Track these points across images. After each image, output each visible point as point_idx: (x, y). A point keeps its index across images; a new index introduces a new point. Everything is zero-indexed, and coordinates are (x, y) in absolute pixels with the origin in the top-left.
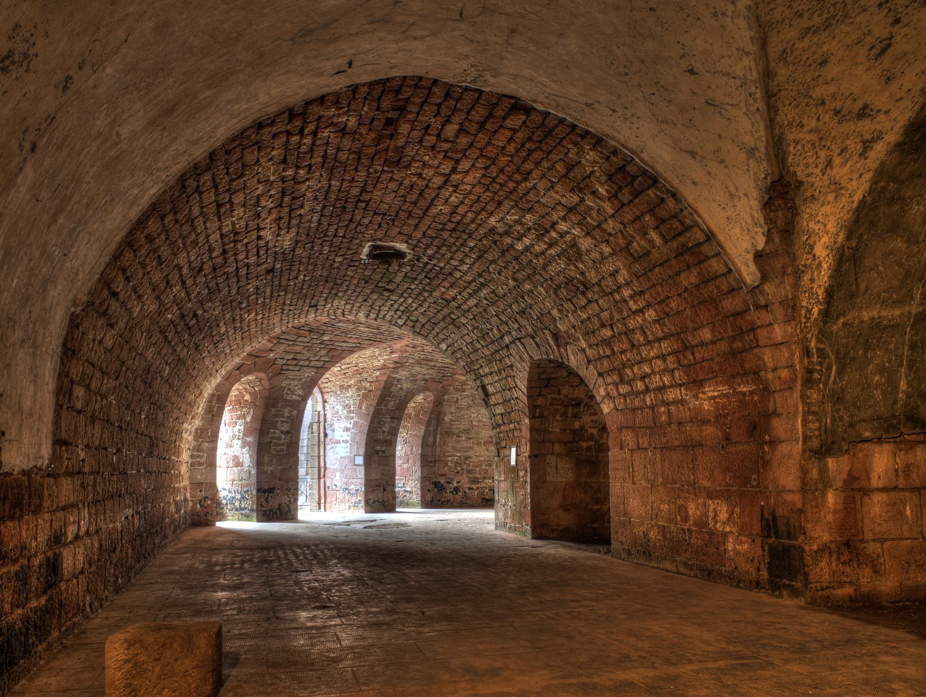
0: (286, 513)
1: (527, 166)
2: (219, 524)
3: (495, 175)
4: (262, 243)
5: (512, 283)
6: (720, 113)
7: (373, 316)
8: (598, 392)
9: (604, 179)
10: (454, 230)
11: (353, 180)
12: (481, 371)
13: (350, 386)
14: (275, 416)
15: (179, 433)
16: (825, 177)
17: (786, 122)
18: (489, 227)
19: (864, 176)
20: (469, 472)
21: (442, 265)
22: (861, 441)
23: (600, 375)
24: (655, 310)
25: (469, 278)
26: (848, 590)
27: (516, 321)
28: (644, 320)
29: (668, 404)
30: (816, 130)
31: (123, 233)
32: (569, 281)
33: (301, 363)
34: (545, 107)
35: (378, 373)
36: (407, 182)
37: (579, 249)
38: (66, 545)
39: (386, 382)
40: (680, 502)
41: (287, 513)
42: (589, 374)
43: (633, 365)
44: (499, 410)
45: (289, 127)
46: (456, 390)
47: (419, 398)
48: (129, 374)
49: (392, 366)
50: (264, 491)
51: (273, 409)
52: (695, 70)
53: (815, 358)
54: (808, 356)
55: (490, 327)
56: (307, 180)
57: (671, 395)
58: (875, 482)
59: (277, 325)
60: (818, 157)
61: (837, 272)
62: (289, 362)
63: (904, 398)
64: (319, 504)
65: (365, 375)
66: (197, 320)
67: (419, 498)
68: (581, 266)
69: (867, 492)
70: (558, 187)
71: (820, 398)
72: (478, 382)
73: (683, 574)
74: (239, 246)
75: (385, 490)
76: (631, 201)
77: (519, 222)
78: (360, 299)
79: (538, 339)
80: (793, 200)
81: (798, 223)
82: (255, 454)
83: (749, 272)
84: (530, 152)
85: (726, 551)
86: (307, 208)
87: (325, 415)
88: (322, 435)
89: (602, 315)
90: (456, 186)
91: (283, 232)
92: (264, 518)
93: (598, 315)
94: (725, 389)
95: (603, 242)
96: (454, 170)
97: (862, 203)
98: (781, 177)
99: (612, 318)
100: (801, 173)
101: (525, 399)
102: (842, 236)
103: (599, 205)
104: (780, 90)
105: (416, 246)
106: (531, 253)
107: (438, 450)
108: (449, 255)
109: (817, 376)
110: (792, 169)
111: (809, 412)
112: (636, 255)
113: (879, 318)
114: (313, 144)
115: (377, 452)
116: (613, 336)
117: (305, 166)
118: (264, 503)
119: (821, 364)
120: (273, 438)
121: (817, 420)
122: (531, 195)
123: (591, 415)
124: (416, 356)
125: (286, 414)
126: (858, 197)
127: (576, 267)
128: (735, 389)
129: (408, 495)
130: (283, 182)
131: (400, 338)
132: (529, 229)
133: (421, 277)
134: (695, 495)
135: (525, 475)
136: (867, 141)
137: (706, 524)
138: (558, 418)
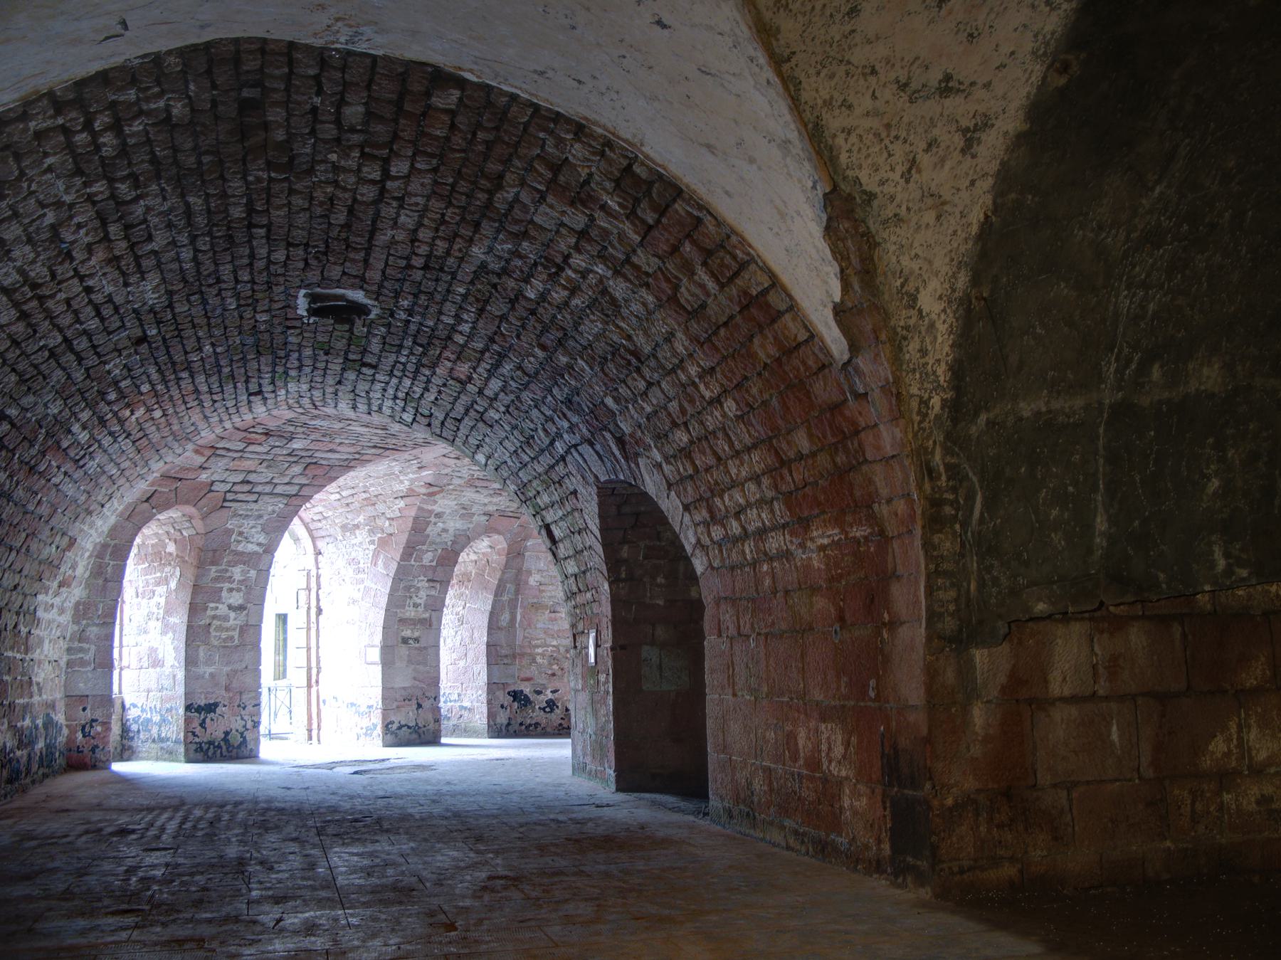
0: (235, 748)
2: (118, 767)
3: (451, 180)
6: (722, 85)
8: (687, 538)
9: (609, 185)
13: (357, 527)
14: (216, 579)
16: (912, 185)
17: (820, 102)
19: (978, 184)
21: (431, 323)
22: (1031, 619)
23: (686, 508)
24: (734, 399)
26: (1009, 871)
27: (565, 415)
28: (724, 415)
29: (771, 559)
30: (875, 113)
32: (615, 350)
33: (259, 489)
34: (478, 77)
35: (402, 504)
37: (613, 301)
39: (416, 519)
40: (788, 728)
41: (239, 747)
42: (670, 505)
43: (723, 491)
44: (571, 567)
45: (60, 121)
47: (483, 545)
49: (423, 490)
50: (199, 709)
51: (214, 568)
52: (665, 21)
53: (943, 481)
54: (931, 478)
56: (138, 198)
57: (775, 543)
58: (1057, 687)
60: (890, 155)
61: (965, 338)
62: (236, 488)
63: (1104, 544)
64: (310, 731)
65: (381, 507)
66: (13, 425)
67: (485, 721)
68: (622, 324)
69: (1042, 704)
70: (550, 199)
71: (958, 549)
73: (792, 849)
74: (50, 304)
75: (419, 706)
76: (658, 222)
77: (516, 254)
78: (330, 380)
79: (598, 447)
80: (863, 221)
81: (880, 259)
82: (182, 645)
83: (834, 339)
84: (489, 145)
85: (841, 808)
87: (318, 577)
88: (313, 611)
89: (670, 405)
92: (200, 756)
93: (666, 408)
95: (641, 286)
96: (386, 175)
97: (986, 223)
98: (835, 188)
99: (683, 411)
100: (869, 182)
101: (599, 548)
102: (963, 280)
103: (618, 228)
104: (794, 53)
107: (520, 634)
109: (948, 510)
110: (850, 173)
111: (937, 572)
112: (689, 308)
113: (1049, 412)
115: (405, 641)
116: (692, 442)
118: (198, 730)
119: (954, 490)
120: (214, 617)
121: (953, 585)
122: (516, 210)
126: (976, 217)
127: (618, 327)
129: (466, 714)
130: (94, 203)
133: (408, 342)
134: (806, 714)
138: (660, 580)
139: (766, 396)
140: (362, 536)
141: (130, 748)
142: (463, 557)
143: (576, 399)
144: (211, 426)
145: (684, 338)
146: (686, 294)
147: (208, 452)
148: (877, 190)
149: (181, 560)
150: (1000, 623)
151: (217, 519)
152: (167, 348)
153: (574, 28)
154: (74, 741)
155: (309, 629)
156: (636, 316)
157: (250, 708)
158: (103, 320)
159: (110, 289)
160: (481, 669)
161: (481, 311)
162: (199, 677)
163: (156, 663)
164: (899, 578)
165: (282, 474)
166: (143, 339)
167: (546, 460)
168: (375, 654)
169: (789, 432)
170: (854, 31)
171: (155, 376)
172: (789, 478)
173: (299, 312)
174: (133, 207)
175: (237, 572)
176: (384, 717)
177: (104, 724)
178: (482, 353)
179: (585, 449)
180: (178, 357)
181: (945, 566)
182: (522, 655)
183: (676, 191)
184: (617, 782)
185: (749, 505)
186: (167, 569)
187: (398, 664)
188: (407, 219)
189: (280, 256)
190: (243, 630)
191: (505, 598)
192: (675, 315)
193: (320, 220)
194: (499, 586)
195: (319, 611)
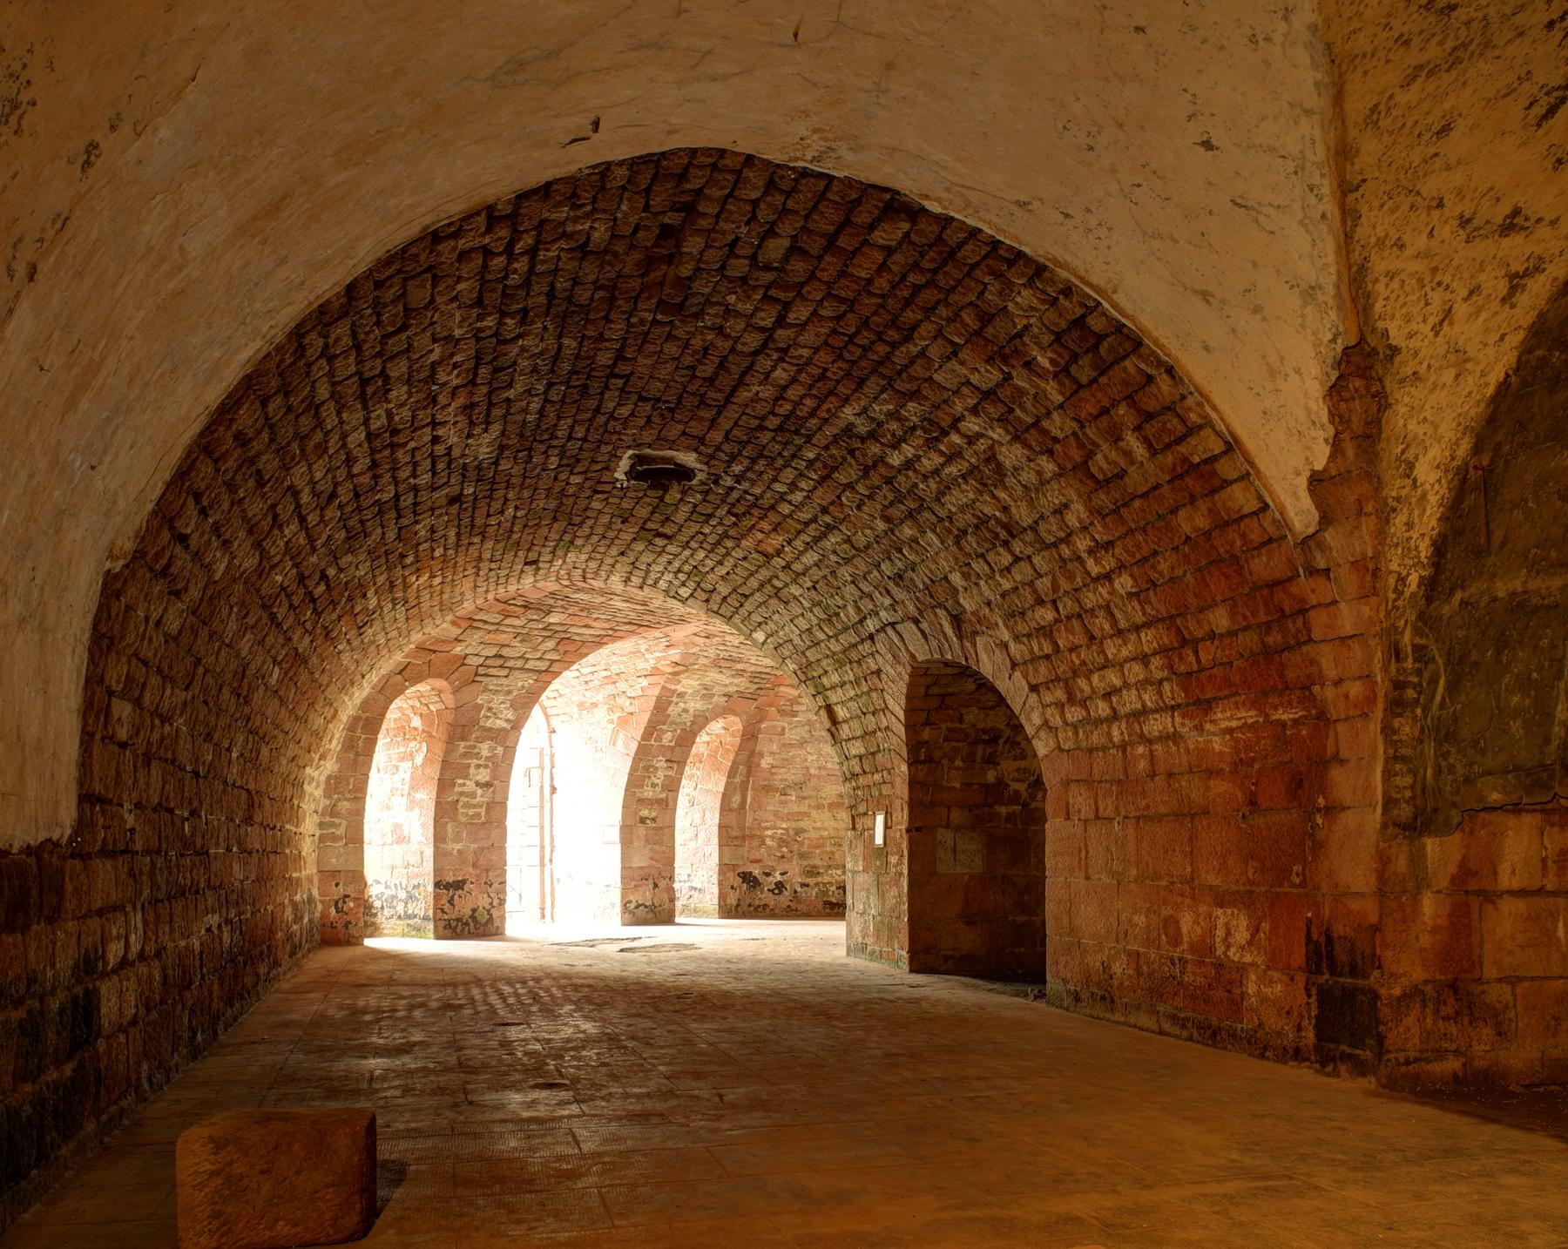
0: (483, 926)
1: (910, 316)
2: (368, 942)
4: (440, 449)
5: (881, 525)
6: (1257, 221)
7: (636, 580)
8: (1029, 719)
9: (1047, 339)
10: (780, 429)
11: (601, 338)
12: (825, 680)
13: (595, 705)
14: (465, 755)
15: (298, 785)
16: (1440, 339)
17: (1373, 240)
18: (842, 424)
19: (1507, 339)
20: (802, 856)
22: (1485, 809)
23: (1034, 688)
24: (1132, 576)
25: (805, 516)
26: (1452, 1065)
27: (888, 592)
28: (1113, 592)
29: (1150, 742)
31: (195, 429)
32: (982, 522)
33: (510, 663)
34: (945, 208)
35: (644, 682)
36: (697, 343)
37: (999, 465)
38: (105, 975)
39: (658, 699)
40: (1167, 911)
41: (486, 924)
42: (1014, 688)
43: (1091, 672)
44: (857, 748)
45: (487, 240)
46: (782, 713)
47: (716, 727)
48: (210, 680)
49: (669, 670)
50: (448, 886)
51: (462, 744)
52: (1214, 142)
53: (1409, 664)
55: (841, 603)
56: (520, 336)
57: (1156, 725)
58: (1506, 881)
59: (469, 595)
60: (1427, 304)
61: (1454, 512)
62: (489, 662)
65: (622, 686)
66: (328, 586)
67: (716, 901)
69: (1489, 897)
70: (964, 354)
72: (819, 698)
73: (1168, 1034)
74: (400, 454)
75: (656, 886)
76: (1094, 381)
77: (894, 416)
78: (614, 551)
80: (1380, 380)
81: (1388, 422)
82: (431, 823)
83: (1300, 511)
84: (917, 289)
86: (519, 387)
87: (552, 756)
88: (547, 790)
89: (1038, 583)
90: (785, 351)
91: (477, 430)
93: (1031, 584)
94: (1251, 716)
96: (781, 322)
99: (1055, 587)
100: (1396, 338)
102: (1466, 445)
103: (1038, 387)
104: (1364, 181)
105: (712, 457)
106: (915, 471)
107: (749, 818)
108: (771, 474)
109: (1411, 693)
111: (1395, 758)
112: (1100, 477)
113: (1525, 592)
114: (531, 271)
115: (643, 820)
116: (1057, 621)
117: (518, 312)
118: (447, 907)
119: (1419, 672)
120: (461, 794)
121: (1409, 771)
123: (1015, 758)
124: (712, 653)
125: (485, 753)
126: (1495, 377)
127: (994, 497)
128: (1267, 716)
129: (696, 894)
130: (478, 340)
131: (683, 620)
132: (913, 429)
134: (1193, 898)
135: (900, 863)
136: (1516, 275)
137: (1211, 949)
138: (958, 763)
139: (1178, 572)
140: (601, 713)
141: (373, 924)
142: (702, 738)
143: (910, 574)
144: (471, 597)
145: (1082, 509)
146: (1101, 463)
147: (464, 624)
148: (1403, 345)
149: (429, 736)
150: (1454, 812)
151: (466, 693)
152: (474, 508)
153: (1091, 148)
154: (328, 916)
155: (542, 808)
156: (1025, 486)
157: (496, 885)
158: (434, 473)
159: (454, 440)
160: (713, 849)
161: (823, 479)
162: (448, 854)
163: (401, 839)
164: (1343, 762)
165: (535, 649)
166: (456, 499)
167: (849, 638)
168: (615, 834)
169: (1201, 610)
170: (1436, 155)
171: (452, 539)
172: (1192, 658)
173: (616, 475)
174: (509, 347)
175: (485, 749)
176: (623, 896)
177: (356, 899)
178: (807, 524)
179: (908, 629)
180: (479, 521)
181: (1403, 751)
182: (752, 837)
183: (1133, 343)
184: (911, 963)
185: (1126, 685)
186: (412, 744)
187: (636, 844)
188: (780, 374)
189: (624, 411)
190: (490, 806)
191: (737, 780)
192: (1079, 485)
193: (684, 372)
194: (732, 768)
195: (553, 790)
